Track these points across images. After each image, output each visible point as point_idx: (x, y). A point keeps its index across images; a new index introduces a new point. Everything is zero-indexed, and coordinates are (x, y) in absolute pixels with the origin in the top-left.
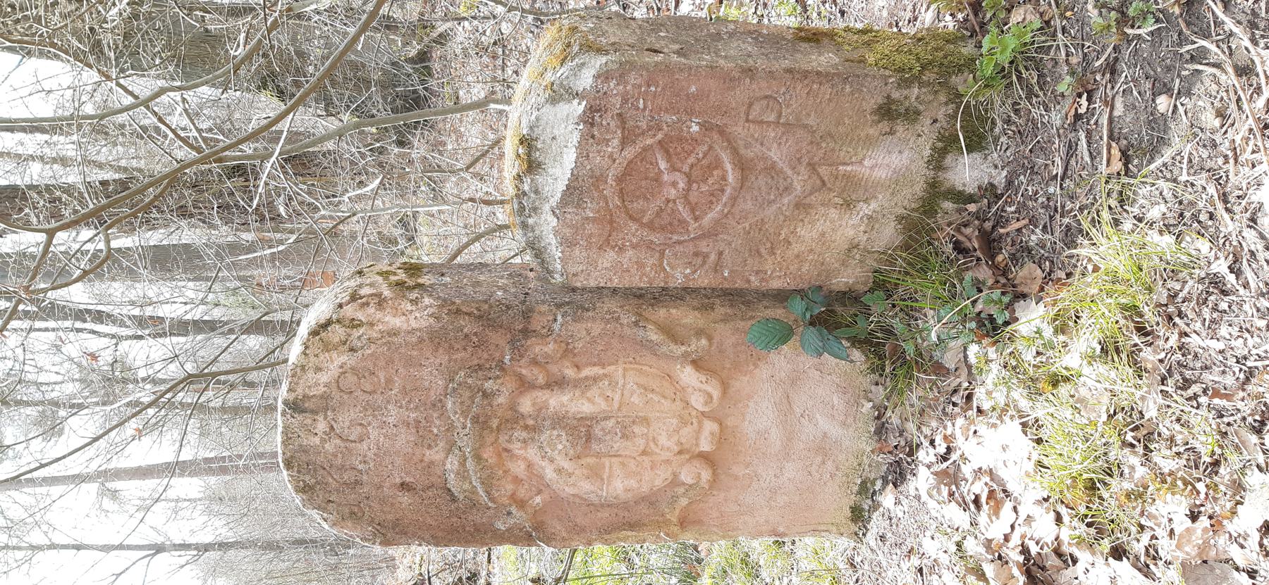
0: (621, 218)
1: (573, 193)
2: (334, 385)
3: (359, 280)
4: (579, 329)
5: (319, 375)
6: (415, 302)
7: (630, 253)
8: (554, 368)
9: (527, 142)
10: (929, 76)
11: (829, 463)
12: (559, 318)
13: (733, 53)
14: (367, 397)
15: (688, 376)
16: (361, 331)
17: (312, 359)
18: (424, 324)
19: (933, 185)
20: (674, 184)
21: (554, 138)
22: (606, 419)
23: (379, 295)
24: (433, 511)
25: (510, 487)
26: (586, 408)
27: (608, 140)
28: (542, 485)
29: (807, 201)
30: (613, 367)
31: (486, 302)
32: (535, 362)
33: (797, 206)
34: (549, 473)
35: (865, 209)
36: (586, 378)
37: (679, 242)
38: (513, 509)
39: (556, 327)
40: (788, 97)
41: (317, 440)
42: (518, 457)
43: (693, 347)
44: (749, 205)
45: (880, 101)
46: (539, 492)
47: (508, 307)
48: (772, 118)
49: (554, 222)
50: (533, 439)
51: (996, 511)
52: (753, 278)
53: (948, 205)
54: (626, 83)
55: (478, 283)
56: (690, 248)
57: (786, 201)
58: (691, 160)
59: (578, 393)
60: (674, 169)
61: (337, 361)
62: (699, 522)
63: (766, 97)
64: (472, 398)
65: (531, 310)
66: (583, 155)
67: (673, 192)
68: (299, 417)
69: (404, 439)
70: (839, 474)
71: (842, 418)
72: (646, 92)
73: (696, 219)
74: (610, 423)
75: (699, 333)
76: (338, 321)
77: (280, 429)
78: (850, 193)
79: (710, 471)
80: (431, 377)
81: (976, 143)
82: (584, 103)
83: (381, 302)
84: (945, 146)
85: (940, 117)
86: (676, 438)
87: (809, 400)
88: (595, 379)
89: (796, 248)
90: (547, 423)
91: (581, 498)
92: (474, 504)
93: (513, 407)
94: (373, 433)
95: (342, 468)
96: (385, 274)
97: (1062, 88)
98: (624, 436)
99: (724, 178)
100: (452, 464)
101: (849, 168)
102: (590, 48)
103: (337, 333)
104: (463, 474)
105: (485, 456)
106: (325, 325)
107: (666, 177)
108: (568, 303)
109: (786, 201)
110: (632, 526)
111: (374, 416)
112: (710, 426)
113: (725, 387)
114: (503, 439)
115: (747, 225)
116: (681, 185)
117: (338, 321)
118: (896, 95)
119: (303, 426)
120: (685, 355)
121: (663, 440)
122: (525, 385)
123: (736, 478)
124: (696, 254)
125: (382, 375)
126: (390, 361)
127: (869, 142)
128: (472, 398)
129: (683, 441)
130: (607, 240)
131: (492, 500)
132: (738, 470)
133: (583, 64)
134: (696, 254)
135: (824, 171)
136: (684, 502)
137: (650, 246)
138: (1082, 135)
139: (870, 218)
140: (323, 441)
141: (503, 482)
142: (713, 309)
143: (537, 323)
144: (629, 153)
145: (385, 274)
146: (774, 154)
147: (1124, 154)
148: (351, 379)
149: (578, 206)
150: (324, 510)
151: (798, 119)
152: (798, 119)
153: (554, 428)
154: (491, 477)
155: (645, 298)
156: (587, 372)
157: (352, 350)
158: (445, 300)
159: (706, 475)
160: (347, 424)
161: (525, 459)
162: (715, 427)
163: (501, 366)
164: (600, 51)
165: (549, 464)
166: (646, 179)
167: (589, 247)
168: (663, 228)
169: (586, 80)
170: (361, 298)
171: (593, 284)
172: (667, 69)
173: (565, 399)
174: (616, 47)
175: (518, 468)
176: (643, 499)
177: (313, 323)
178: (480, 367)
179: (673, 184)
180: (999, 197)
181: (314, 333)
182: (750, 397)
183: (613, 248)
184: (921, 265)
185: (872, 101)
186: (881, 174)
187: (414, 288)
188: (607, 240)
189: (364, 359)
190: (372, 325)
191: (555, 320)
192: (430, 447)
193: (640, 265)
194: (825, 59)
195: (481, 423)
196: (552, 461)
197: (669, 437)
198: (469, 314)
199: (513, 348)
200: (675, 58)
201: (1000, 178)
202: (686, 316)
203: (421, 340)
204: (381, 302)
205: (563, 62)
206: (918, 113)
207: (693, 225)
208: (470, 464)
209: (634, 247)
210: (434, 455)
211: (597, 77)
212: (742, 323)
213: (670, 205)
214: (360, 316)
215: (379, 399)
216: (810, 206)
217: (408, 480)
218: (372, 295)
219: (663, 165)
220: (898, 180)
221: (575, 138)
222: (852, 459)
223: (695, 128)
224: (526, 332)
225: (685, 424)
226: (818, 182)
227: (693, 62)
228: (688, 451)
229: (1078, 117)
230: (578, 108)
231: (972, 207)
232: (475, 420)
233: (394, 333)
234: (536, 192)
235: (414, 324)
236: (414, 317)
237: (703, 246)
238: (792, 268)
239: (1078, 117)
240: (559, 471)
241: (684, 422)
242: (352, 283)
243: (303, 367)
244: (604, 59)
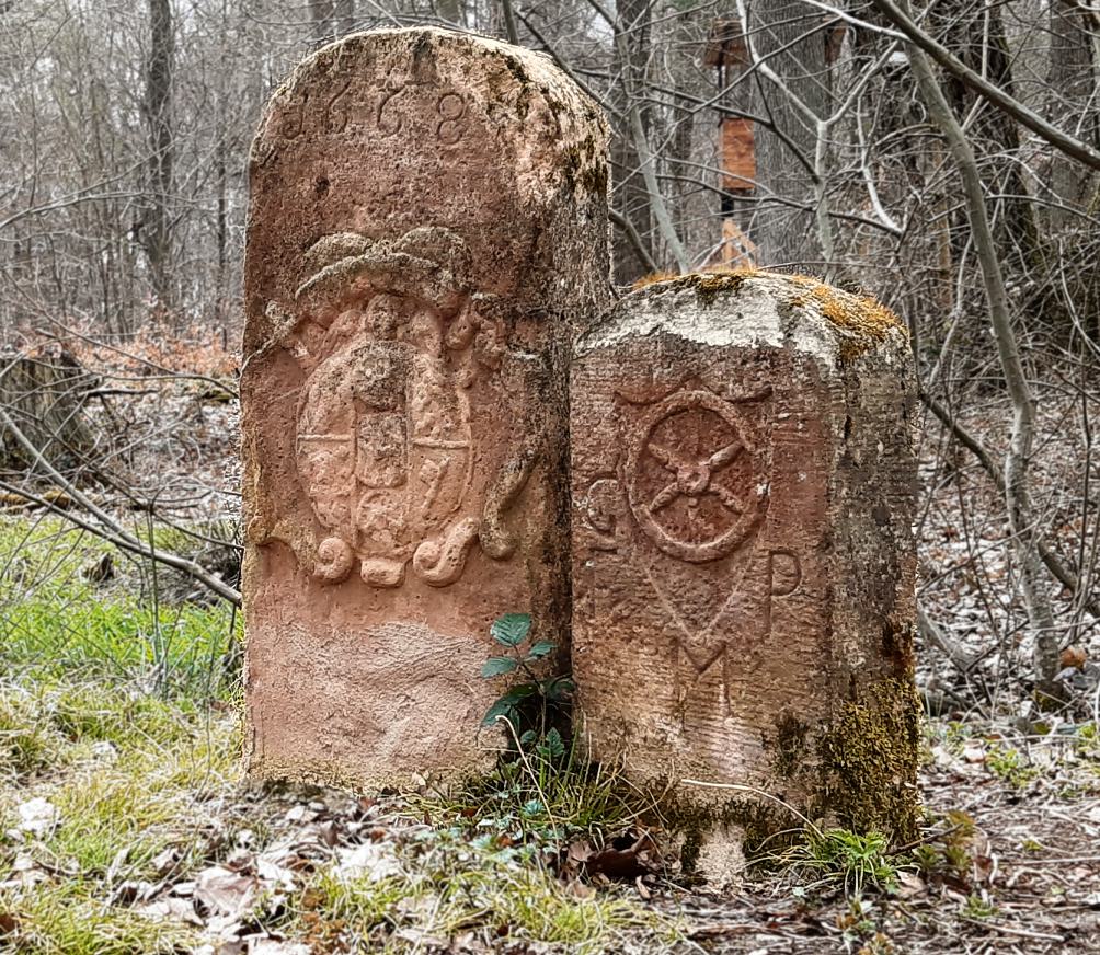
0: (652, 414)
1: (679, 349)
2: (448, 90)
3: (580, 114)
5: (459, 72)
6: (550, 179)
7: (611, 433)
8: (467, 358)
10: (834, 777)
11: (345, 742)
12: (531, 356)
14: (432, 130)
15: (459, 532)
16: (514, 118)
17: (480, 62)
18: (522, 190)
20: (695, 476)
21: (740, 316)
22: (404, 429)
26: (417, 402)
27: (741, 382)
29: (681, 653)
30: (469, 433)
31: (551, 264)
32: (476, 329)
33: (675, 641)
34: (335, 362)
36: (455, 399)
37: (625, 496)
39: (520, 354)
40: (801, 598)
42: (356, 321)
43: (495, 534)
46: (312, 354)
49: (645, 330)
50: (378, 338)
52: (584, 601)
53: (681, 839)
54: (804, 392)
55: (577, 259)
57: (680, 624)
58: (724, 492)
60: (714, 471)
62: (269, 570)
63: (799, 573)
67: (686, 475)
69: (381, 179)
71: (405, 751)
72: (796, 418)
73: (655, 512)
74: (397, 436)
76: (526, 90)
77: (395, 31)
78: (691, 710)
79: (334, 575)
82: (780, 345)
83: (549, 139)
86: (378, 526)
89: (624, 652)
91: (303, 408)
92: (298, 273)
93: (420, 305)
94: (388, 141)
96: (589, 144)
99: (705, 539)
100: (350, 239)
101: (721, 699)
102: (847, 353)
103: (512, 90)
104: (337, 253)
105: (359, 279)
106: (520, 74)
107: (703, 463)
108: (550, 367)
109: (680, 624)
111: (410, 140)
112: (393, 570)
115: (650, 580)
116: (694, 485)
117: (526, 90)
118: (809, 738)
120: (485, 525)
121: (376, 509)
122: (447, 318)
123: (326, 616)
124: (612, 520)
125: (460, 144)
126: (476, 153)
128: (430, 256)
129: (375, 536)
131: (304, 293)
133: (823, 338)
137: (620, 458)
139: (663, 741)
141: (326, 304)
142: (546, 561)
143: (525, 331)
144: (729, 411)
145: (589, 144)
146: (735, 595)
149: (664, 357)
150: (296, 91)
151: (778, 616)
152: (778, 616)
153: (392, 362)
155: (554, 466)
156: (463, 398)
157: (491, 107)
158: (551, 214)
159: (329, 570)
160: (401, 109)
161: (354, 331)
162: (392, 580)
165: (346, 361)
166: (700, 438)
167: (618, 379)
168: (641, 470)
169: (805, 343)
170: (555, 115)
171: (573, 392)
172: (825, 439)
173: (429, 373)
175: (342, 322)
177: (525, 61)
179: (692, 475)
181: (511, 63)
183: (617, 410)
185: (801, 711)
187: (569, 178)
190: (521, 129)
191: (528, 352)
192: (371, 211)
193: (597, 449)
195: (400, 269)
196: (351, 363)
198: (534, 246)
200: (839, 451)
202: (534, 522)
203: (502, 188)
204: (549, 139)
207: (647, 509)
208: (350, 260)
209: (619, 437)
211: (810, 356)
212: (527, 601)
213: (671, 476)
214: (532, 115)
216: (675, 659)
217: (331, 188)
218: (559, 127)
219: (717, 457)
220: (706, 767)
221: (742, 342)
222: (349, 772)
223: (760, 489)
225: (396, 538)
226: (704, 662)
228: (361, 545)
230: (775, 340)
231: (677, 865)
232: (403, 262)
233: (511, 154)
235: (521, 178)
238: (598, 650)
240: (338, 375)
241: (400, 535)
242: (576, 105)
243: (469, 52)
244: (830, 361)
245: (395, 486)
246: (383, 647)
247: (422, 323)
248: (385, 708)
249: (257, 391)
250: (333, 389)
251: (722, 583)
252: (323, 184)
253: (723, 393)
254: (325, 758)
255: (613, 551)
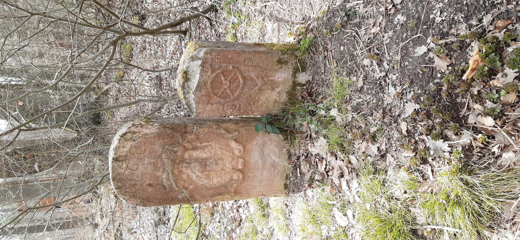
0: (212, 95)
1: (199, 87)
4: (201, 130)
5: (124, 149)
7: (215, 105)
8: (194, 143)
9: (186, 73)
10: (289, 52)
11: (276, 170)
12: (195, 127)
13: (238, 48)
14: (138, 155)
15: (233, 144)
18: (155, 131)
19: (294, 82)
20: (226, 84)
22: (210, 159)
23: (141, 124)
24: (158, 193)
25: (183, 182)
26: (204, 156)
28: (192, 182)
32: (188, 142)
33: (259, 90)
34: (194, 177)
35: (278, 90)
37: (229, 102)
38: (184, 191)
39: (194, 130)
41: (123, 170)
42: (185, 173)
43: (234, 135)
44: (247, 90)
45: (278, 59)
46: (191, 185)
47: (180, 125)
48: (251, 64)
49: (193, 96)
51: (322, 162)
53: (298, 88)
56: (231, 103)
59: (202, 151)
61: (129, 144)
62: (239, 193)
64: (170, 153)
65: (186, 126)
66: (201, 76)
68: (118, 163)
69: (150, 169)
70: (279, 173)
73: (233, 95)
74: (212, 160)
75: (236, 130)
76: (129, 132)
78: (273, 85)
80: (158, 147)
81: (304, 70)
83: (142, 126)
84: (296, 71)
85: (293, 63)
87: (268, 151)
88: (207, 146)
89: (260, 102)
90: (193, 161)
94: (140, 167)
95: (131, 180)
97: (320, 50)
98: (216, 164)
99: (239, 82)
100: (165, 176)
103: (129, 136)
104: (168, 179)
107: (224, 82)
110: (220, 194)
112: (241, 160)
113: (244, 147)
114: (180, 166)
116: (228, 84)
117: (129, 132)
118: (281, 57)
119: (119, 166)
120: (233, 137)
121: (227, 165)
122: (186, 149)
123: (250, 177)
124: (233, 105)
125: (143, 148)
126: (145, 143)
127: (276, 71)
128: (170, 153)
130: (208, 102)
131: (177, 187)
132: (250, 175)
134: (233, 105)
135: (265, 79)
136: (235, 185)
137: (220, 103)
138: (327, 61)
139: (279, 92)
140: (125, 171)
141: (181, 181)
143: (189, 129)
146: (252, 75)
147: (336, 62)
148: (134, 149)
149: (200, 91)
150: (124, 195)
154: (177, 179)
155: (219, 122)
156: (204, 144)
157: (134, 140)
159: (241, 176)
162: (242, 160)
163: (178, 143)
164: (204, 47)
165: (193, 174)
167: (203, 104)
168: (224, 98)
169: (202, 54)
173: (198, 153)
174: (208, 46)
175: (185, 177)
176: (223, 185)
178: (172, 144)
179: (226, 84)
180: (311, 83)
181: (122, 136)
182: (252, 151)
184: (293, 104)
186: (280, 79)
188: (208, 102)
189: (138, 143)
190: (140, 132)
192: (158, 171)
193: (218, 109)
194: (262, 49)
195: (173, 161)
196: (195, 173)
197: (229, 164)
199: (182, 137)
201: (310, 78)
203: (155, 136)
204: (142, 126)
205: (195, 51)
206: (288, 62)
208: (170, 175)
209: (216, 103)
210: (159, 174)
211: (204, 54)
214: (136, 130)
215: (142, 155)
216: (263, 90)
217: (151, 182)
219: (223, 79)
220: (285, 81)
221: (199, 71)
222: (282, 168)
223: (231, 68)
224: (185, 132)
227: (229, 49)
229: (325, 57)
230: (200, 62)
231: (305, 87)
232: (172, 160)
233: (146, 134)
234: (188, 87)
235: (152, 131)
236: (152, 130)
237: (235, 103)
239: (325, 57)
240: (197, 176)
241: (233, 159)
245: (223, 161)
246: (256, 162)
247: (186, 156)
248: (269, 161)
249: (200, 198)
250: (201, 178)
251: (249, 78)
252: (150, 185)
253: (210, 75)
254: (280, 175)
255: (240, 105)
